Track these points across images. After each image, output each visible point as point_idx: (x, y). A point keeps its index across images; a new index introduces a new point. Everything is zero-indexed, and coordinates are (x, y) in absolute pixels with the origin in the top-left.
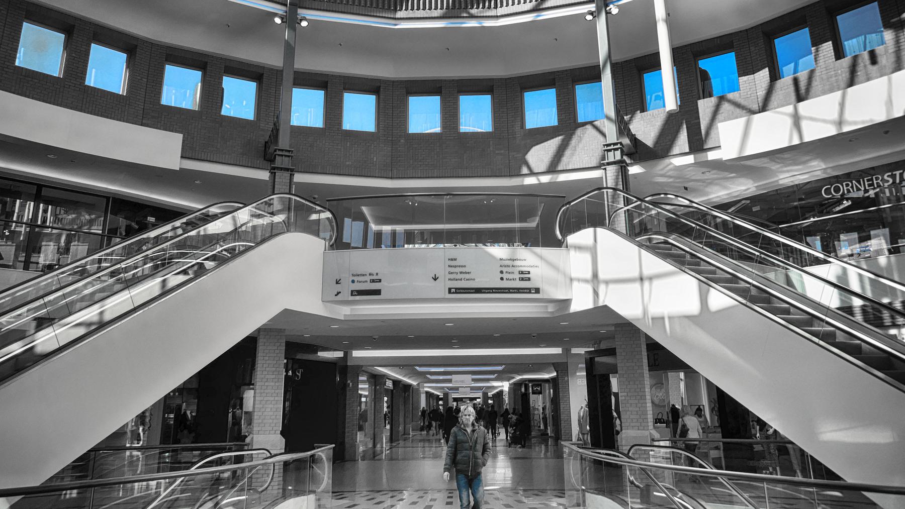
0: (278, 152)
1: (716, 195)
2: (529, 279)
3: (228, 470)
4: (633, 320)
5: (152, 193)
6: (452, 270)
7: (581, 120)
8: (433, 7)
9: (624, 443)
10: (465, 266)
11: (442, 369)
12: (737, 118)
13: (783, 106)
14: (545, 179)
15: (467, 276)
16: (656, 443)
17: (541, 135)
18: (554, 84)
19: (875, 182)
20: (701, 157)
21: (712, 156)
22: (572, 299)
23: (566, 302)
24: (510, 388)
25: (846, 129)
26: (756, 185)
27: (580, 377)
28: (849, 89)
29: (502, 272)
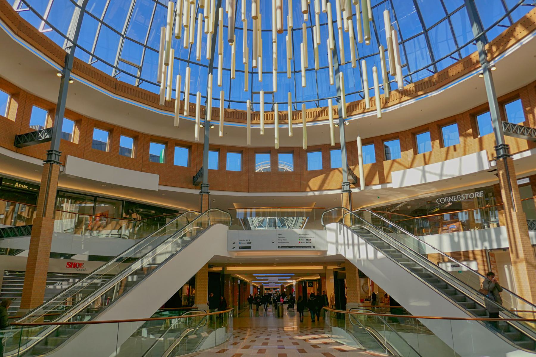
0: (203, 185)
2: (311, 243)
3: (194, 316)
4: (350, 260)
8: (268, 119)
9: (348, 308)
14: (317, 193)
15: (286, 241)
16: (360, 308)
17: (316, 173)
19: (458, 198)
20: (384, 185)
21: (389, 186)
22: (327, 251)
23: (325, 252)
24: (296, 284)
25: (444, 178)
26: (409, 197)
27: (331, 279)
28: (446, 162)
29: (300, 240)
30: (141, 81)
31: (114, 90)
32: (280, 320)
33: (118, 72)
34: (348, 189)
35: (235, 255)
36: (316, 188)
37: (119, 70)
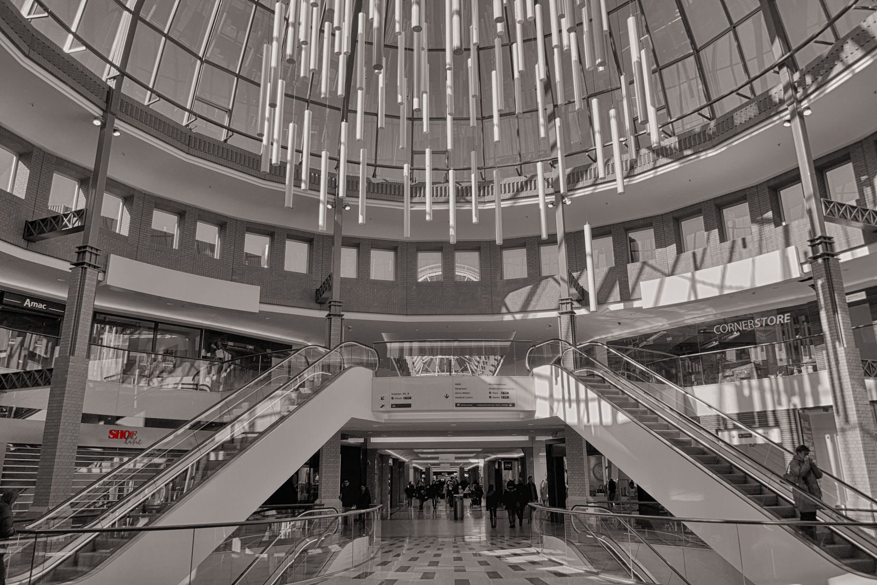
0: (332, 303)
1: (641, 328)
2: (508, 397)
5: (231, 325)
6: (458, 391)
7: (544, 274)
8: (439, 195)
10: (460, 384)
11: (433, 451)
12: (653, 279)
13: (685, 272)
14: (518, 317)
15: (467, 395)
16: (589, 505)
17: (516, 284)
18: (525, 246)
20: (628, 304)
21: (636, 304)
23: (533, 413)
24: (485, 465)
25: (726, 292)
26: (669, 322)
27: (542, 456)
28: (729, 265)
29: (490, 393)
30: (230, 133)
31: (185, 148)
32: (459, 524)
33: (194, 118)
34: (569, 309)
35: (384, 418)
36: (517, 309)
37: (195, 114)
